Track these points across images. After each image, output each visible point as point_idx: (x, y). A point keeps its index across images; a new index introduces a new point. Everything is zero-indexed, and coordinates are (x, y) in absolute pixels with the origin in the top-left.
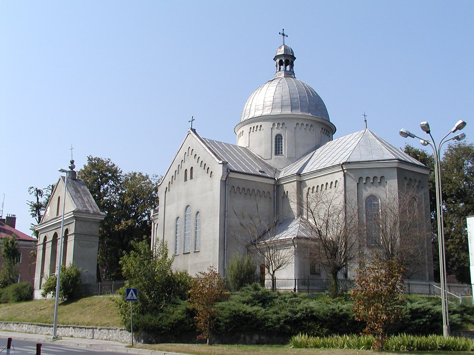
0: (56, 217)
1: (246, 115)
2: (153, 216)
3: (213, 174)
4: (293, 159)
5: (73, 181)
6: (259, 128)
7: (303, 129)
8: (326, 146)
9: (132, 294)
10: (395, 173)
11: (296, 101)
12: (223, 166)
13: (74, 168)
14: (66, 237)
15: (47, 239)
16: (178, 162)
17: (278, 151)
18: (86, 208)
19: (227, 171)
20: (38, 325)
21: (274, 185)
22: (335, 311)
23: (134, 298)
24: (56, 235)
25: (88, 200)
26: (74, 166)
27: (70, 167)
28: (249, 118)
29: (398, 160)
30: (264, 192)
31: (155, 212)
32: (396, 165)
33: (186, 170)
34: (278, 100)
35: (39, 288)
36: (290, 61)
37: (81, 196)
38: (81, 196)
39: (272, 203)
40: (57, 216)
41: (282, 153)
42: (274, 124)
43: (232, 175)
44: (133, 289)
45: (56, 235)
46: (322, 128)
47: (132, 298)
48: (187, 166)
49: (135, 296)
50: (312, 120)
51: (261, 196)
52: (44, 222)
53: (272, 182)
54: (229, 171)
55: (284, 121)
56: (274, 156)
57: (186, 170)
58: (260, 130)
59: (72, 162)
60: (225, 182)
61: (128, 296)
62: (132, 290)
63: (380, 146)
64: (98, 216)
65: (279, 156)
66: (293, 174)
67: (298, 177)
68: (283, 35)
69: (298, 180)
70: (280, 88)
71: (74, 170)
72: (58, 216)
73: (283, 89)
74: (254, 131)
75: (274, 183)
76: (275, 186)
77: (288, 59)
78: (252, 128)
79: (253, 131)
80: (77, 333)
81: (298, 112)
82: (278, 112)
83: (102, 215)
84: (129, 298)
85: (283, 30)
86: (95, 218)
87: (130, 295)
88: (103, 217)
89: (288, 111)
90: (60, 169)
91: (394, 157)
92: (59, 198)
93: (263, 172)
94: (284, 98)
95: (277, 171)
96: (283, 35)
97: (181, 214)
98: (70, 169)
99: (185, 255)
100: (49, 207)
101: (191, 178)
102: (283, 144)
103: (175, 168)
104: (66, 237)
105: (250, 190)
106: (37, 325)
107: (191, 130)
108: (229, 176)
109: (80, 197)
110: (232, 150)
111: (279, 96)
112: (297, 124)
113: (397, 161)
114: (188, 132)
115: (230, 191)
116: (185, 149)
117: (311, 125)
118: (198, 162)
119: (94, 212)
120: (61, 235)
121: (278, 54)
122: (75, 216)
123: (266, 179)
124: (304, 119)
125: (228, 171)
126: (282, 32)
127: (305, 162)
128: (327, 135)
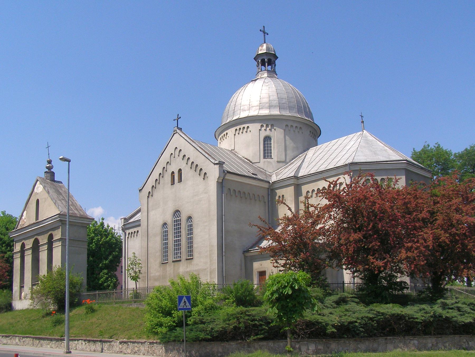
0: (34, 221)
1: (229, 116)
2: (123, 225)
3: (207, 175)
4: (284, 162)
5: (51, 182)
7: (296, 131)
8: (317, 149)
9: (185, 302)
11: (284, 101)
17: (267, 153)
18: (72, 211)
20: (36, 338)
21: (268, 189)
22: (86, 308)
23: (188, 307)
24: (36, 242)
26: (53, 166)
27: (47, 168)
28: (233, 119)
29: (406, 160)
30: (254, 195)
31: (125, 221)
32: (404, 166)
33: (173, 173)
34: (266, 100)
35: (19, 298)
37: (64, 199)
38: (64, 199)
39: (267, 208)
40: (36, 221)
42: (262, 126)
43: (229, 177)
44: (185, 296)
45: (36, 242)
46: (310, 131)
47: (185, 307)
48: (174, 168)
49: (189, 305)
51: (256, 200)
52: (20, 228)
53: (266, 185)
55: (273, 122)
56: (262, 160)
57: (173, 173)
58: (246, 132)
60: (221, 184)
62: (185, 298)
63: (383, 147)
67: (295, 180)
68: (264, 32)
69: (296, 183)
70: (266, 87)
72: (38, 221)
75: (268, 187)
76: (269, 190)
78: (246, 128)
79: (239, 134)
81: (287, 113)
82: (265, 112)
84: (182, 307)
85: (264, 27)
87: (182, 304)
89: (276, 112)
91: (402, 159)
92: (38, 201)
93: (256, 175)
94: (271, 98)
96: (264, 32)
97: (169, 219)
98: (47, 170)
99: (188, 261)
101: (180, 180)
102: (272, 147)
103: (158, 170)
106: (33, 338)
107: (177, 129)
108: (226, 177)
109: (63, 200)
110: (219, 151)
111: (267, 96)
112: (287, 126)
114: (174, 131)
115: (227, 194)
117: (301, 128)
118: (187, 164)
119: (80, 215)
120: (43, 240)
121: (259, 53)
122: (61, 219)
123: (260, 182)
125: (224, 173)
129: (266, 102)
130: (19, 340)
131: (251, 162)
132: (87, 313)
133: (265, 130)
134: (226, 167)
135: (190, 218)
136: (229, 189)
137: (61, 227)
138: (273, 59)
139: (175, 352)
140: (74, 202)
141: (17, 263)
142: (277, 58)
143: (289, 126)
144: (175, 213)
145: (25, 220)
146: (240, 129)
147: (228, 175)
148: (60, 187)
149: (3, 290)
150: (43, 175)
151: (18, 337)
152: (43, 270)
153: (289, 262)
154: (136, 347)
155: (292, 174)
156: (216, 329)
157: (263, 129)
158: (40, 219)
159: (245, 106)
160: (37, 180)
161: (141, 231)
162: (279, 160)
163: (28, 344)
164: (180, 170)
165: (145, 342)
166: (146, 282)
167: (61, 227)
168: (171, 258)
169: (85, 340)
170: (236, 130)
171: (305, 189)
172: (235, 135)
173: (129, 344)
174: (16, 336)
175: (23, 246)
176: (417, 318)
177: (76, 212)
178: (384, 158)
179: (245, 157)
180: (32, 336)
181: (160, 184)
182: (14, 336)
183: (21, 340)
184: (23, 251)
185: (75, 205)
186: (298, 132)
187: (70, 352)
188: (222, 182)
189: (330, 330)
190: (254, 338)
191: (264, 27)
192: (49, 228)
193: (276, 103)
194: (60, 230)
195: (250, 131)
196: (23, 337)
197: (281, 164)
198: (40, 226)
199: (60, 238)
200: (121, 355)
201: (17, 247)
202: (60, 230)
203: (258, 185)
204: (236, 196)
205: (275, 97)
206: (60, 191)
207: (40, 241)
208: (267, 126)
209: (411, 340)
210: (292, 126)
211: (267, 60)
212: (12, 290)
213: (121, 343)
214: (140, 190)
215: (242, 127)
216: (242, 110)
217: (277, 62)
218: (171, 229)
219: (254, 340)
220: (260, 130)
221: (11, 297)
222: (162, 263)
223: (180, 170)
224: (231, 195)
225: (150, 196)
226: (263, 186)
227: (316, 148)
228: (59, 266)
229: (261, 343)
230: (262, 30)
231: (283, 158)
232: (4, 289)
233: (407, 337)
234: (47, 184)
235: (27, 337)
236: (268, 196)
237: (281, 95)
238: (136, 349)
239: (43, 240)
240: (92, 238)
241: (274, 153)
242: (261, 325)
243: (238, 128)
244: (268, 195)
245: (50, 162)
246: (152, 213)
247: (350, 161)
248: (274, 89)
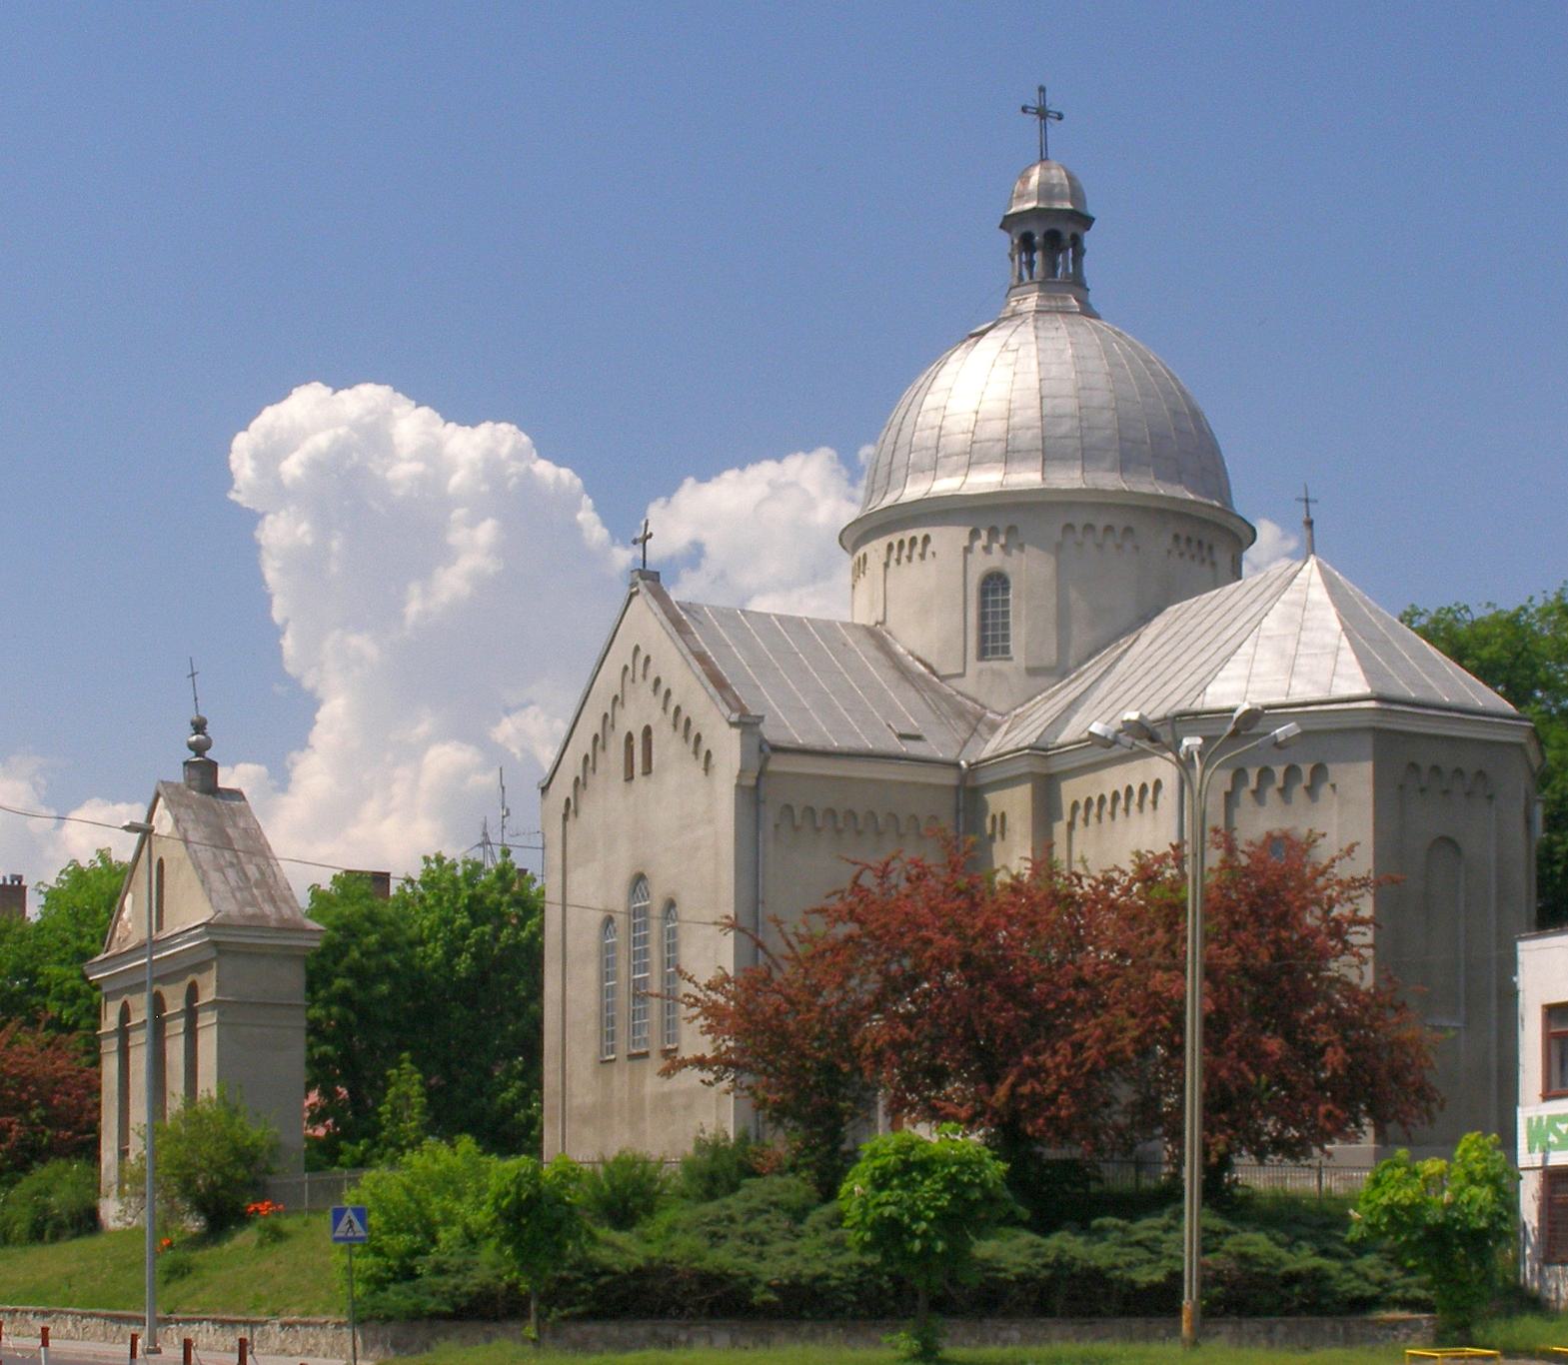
3: (714, 759)
5: (204, 796)
6: (919, 548)
9: (350, 1221)
10: (1368, 743)
12: (742, 734)
13: (208, 748)
14: (191, 1014)
15: (132, 1016)
16: (599, 704)
17: (992, 640)
18: (252, 906)
19: (761, 750)
21: (957, 788)
24: (158, 1003)
25: (262, 874)
27: (191, 746)
33: (630, 737)
34: (996, 428)
36: (1067, 236)
37: (235, 861)
38: (235, 861)
41: (1006, 650)
42: (974, 534)
43: (778, 764)
44: (354, 1210)
46: (1176, 537)
47: (350, 1234)
48: (630, 721)
49: (360, 1228)
50: (1125, 506)
53: (949, 778)
54: (767, 749)
56: (974, 666)
57: (630, 737)
59: (199, 726)
60: (753, 794)
61: (339, 1229)
62: (349, 1214)
64: (306, 936)
65: (996, 665)
66: (999, 756)
68: (1043, 113)
71: (209, 754)
73: (1018, 376)
74: (904, 560)
76: (961, 796)
77: (1053, 226)
78: (907, 543)
80: (222, 1339)
83: (311, 930)
84: (342, 1235)
85: (1042, 90)
86: (287, 943)
87: (343, 1226)
88: (317, 936)
89: (1027, 477)
90: (127, 823)
95: (977, 723)
96: (1043, 113)
97: (618, 900)
98: (193, 754)
99: (606, 1065)
100: (129, 897)
101: (648, 770)
103: (590, 724)
104: (191, 1014)
105: (856, 818)
106: (106, 1317)
107: (639, 579)
108: (772, 767)
109: (232, 865)
112: (1069, 527)
113: (1372, 704)
115: (776, 826)
116: (620, 656)
117: (1128, 530)
120: (175, 1003)
124: (1093, 504)
126: (1033, 100)
127: (1077, 693)
128: (1203, 560)
129: (998, 437)
130: (75, 1325)
131: (934, 672)
132: (261, 1244)
133: (987, 549)
134: (770, 733)
135: (671, 905)
136: (789, 807)
137: (215, 964)
138: (1067, 230)
139: (379, 1347)
140: (268, 872)
141: (110, 1067)
142: (1087, 222)
143: (1079, 529)
144: (637, 884)
145: (130, 926)
146: (913, 541)
147: (774, 757)
148: (233, 813)
149: (71, 1164)
150: (178, 776)
151: (72, 1313)
152: (175, 1103)
153: (1055, 1052)
154: (312, 1335)
155: (1031, 739)
156: (464, 1289)
157: (979, 544)
158: (166, 933)
159: (924, 452)
160: (157, 796)
161: (876, 822)
162: (1031, 664)
163: (94, 1335)
164: (647, 731)
165: (327, 1322)
166: (557, 1128)
167: (215, 964)
168: (623, 1047)
169: (214, 1321)
170: (890, 546)
171: (1072, 791)
172: (886, 565)
173: (299, 1328)
174: (67, 1313)
175: (125, 1014)
176: (1005, 1270)
177: (268, 909)
178: (1309, 688)
179: (918, 653)
180: (104, 1311)
181: (597, 771)
182: (61, 1312)
183: (80, 1326)
184: (123, 1033)
185: (271, 881)
186: (1119, 547)
187: (159, 1351)
188: (757, 787)
189: (760, 1296)
190: (561, 1314)
191: (1042, 90)
192: (188, 963)
193: (1029, 438)
194: (213, 973)
195: (934, 554)
196: (84, 1316)
197: (1041, 681)
198: (164, 954)
199: (210, 999)
200: (283, 1359)
201: (110, 1021)
202: (213, 973)
203: (911, 779)
204: (818, 830)
205: (1033, 413)
206: (230, 831)
207: (168, 1002)
208: (993, 533)
209: (1000, 1329)
210: (1089, 527)
211: (1042, 240)
212: (98, 1158)
213: (283, 1326)
214: (544, 790)
215: (907, 535)
216: (914, 465)
217: (1089, 239)
218: (620, 938)
219: (564, 1318)
220: (967, 550)
221: (96, 1187)
222: (602, 1062)
223: (647, 731)
224: (796, 829)
225: (571, 816)
226: (932, 780)
227: (1179, 609)
228: (208, 1090)
229: (587, 1328)
230: (1029, 104)
231: (1050, 655)
232: (72, 1157)
233: (988, 1322)
234: (188, 807)
235: (92, 1316)
236: (957, 817)
237: (1056, 401)
238: (312, 1341)
239: (175, 1003)
240: (464, 934)
241: (1019, 634)
242: (579, 1280)
243: (895, 538)
244: (957, 811)
245: (199, 726)
246: (576, 878)
247: (1184, 706)
248: (1033, 381)
